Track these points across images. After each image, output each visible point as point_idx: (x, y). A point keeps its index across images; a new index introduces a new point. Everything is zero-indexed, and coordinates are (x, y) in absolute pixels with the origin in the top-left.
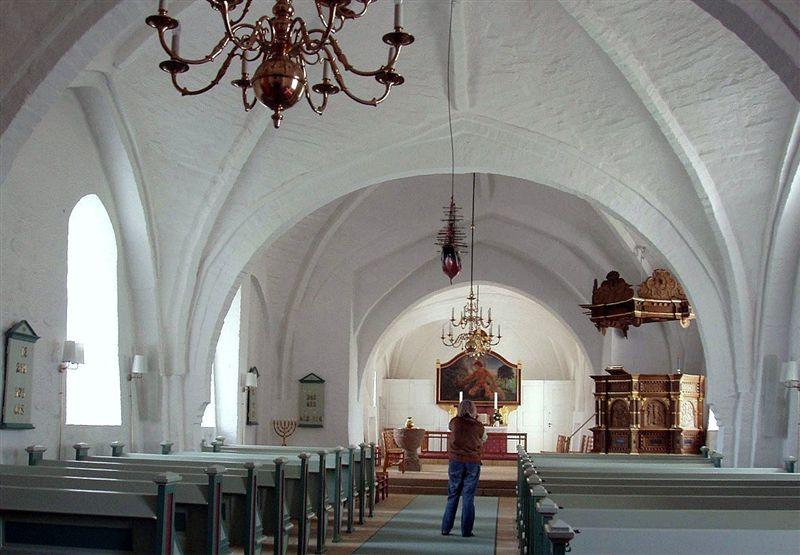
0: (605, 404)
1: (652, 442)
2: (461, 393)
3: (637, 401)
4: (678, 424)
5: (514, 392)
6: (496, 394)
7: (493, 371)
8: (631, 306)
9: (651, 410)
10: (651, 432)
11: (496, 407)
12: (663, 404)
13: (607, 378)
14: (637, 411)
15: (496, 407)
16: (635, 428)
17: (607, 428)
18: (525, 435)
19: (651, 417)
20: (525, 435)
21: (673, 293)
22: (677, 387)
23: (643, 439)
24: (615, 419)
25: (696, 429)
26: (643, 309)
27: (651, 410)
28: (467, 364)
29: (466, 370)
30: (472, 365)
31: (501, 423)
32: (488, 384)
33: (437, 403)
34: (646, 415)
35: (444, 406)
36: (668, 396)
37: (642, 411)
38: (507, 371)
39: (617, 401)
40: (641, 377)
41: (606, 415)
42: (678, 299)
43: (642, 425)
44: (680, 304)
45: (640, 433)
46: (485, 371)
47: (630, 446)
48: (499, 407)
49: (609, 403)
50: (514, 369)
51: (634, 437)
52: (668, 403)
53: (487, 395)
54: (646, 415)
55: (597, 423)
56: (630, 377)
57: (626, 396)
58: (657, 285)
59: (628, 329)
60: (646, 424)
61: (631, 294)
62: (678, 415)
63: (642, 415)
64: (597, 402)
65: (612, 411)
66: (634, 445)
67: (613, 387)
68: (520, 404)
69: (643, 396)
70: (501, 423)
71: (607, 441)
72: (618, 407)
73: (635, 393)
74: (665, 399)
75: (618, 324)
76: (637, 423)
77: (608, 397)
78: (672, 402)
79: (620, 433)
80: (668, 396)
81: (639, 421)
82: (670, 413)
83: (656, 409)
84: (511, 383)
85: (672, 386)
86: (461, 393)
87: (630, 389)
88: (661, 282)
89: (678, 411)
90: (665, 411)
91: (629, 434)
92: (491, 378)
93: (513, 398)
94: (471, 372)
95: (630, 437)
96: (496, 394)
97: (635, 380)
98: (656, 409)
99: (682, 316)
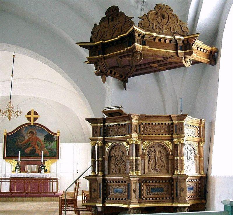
0: (102, 149)
1: (154, 190)
2: (20, 152)
3: (137, 145)
4: (182, 169)
5: (54, 150)
6: (43, 152)
7: (41, 138)
8: (132, 35)
9: (152, 155)
10: (153, 179)
11: (42, 161)
12: (165, 148)
13: (104, 120)
14: (137, 156)
15: (42, 161)
16: (134, 175)
17: (104, 175)
18: (56, 179)
19: (152, 162)
20: (56, 179)
21: (177, 29)
22: (180, 129)
23: (144, 188)
24: (113, 166)
25: (198, 175)
26: (144, 43)
27: (152, 155)
28: (24, 133)
29: (24, 137)
30: (27, 133)
31: (46, 171)
32: (38, 146)
33: (4, 158)
34: (146, 161)
35: (8, 160)
36: (171, 140)
37: (143, 156)
38: (50, 137)
39: (115, 146)
40: (142, 117)
41: (103, 161)
42: (181, 35)
43: (143, 172)
44: (183, 41)
45: (141, 181)
46: (36, 137)
47: (129, 196)
48: (45, 161)
49: (107, 148)
50: (55, 137)
51: (133, 186)
52: (170, 146)
53: (37, 152)
54: (146, 161)
55: (94, 170)
56: (129, 118)
57: (125, 140)
58: (159, 19)
59: (127, 81)
60: (147, 171)
61: (132, 24)
62: (182, 160)
63: (143, 160)
64: (94, 147)
65: (110, 157)
66: (133, 195)
67: (111, 131)
68: (58, 158)
69: (144, 140)
70: (46, 171)
71: (104, 190)
72: (116, 152)
73: (135, 136)
74: (167, 142)
75: (118, 75)
76: (137, 169)
77: (105, 142)
78: (175, 146)
79: (118, 181)
80: (171, 140)
81: (140, 167)
82: (172, 159)
83: (158, 155)
84: (53, 145)
85: (174, 127)
86: (20, 152)
87: (129, 132)
88: (163, 17)
89: (182, 155)
90: (167, 156)
91: (128, 183)
92: (40, 142)
93: (54, 155)
94: (27, 138)
95: (129, 185)
96: (43, 152)
97: (135, 122)
98: (158, 155)
99: (185, 54)
